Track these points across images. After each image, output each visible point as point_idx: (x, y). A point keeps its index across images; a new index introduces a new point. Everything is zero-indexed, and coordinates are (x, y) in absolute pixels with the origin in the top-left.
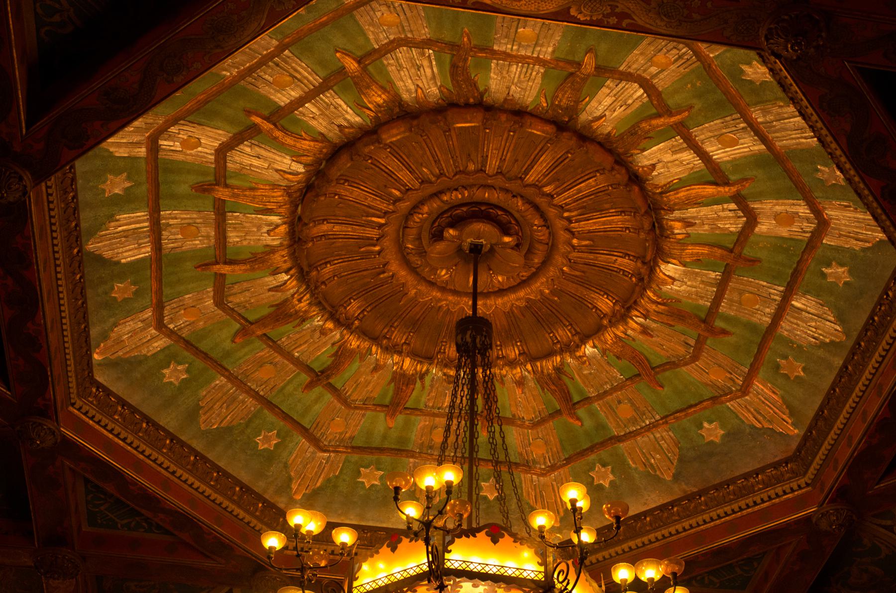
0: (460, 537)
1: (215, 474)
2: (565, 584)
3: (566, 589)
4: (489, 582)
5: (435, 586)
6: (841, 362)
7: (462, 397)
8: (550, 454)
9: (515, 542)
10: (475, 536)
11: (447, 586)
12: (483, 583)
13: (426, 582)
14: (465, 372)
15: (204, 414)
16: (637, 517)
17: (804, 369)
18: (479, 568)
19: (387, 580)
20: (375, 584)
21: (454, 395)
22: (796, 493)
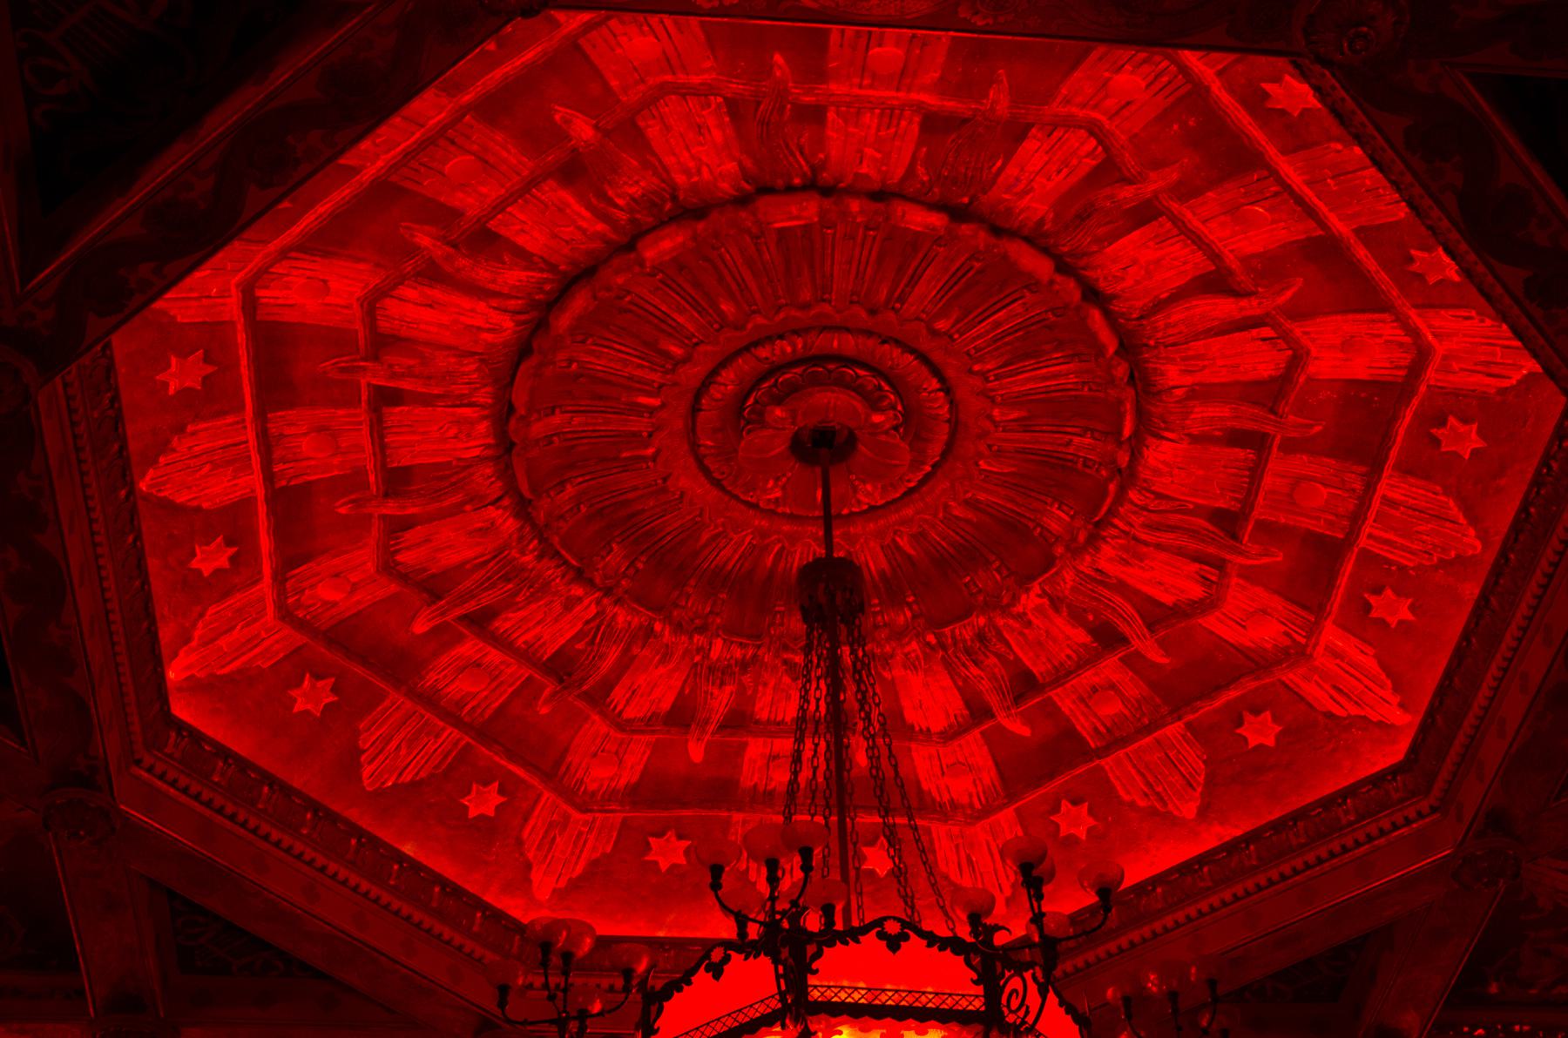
2: (1021, 1013)
3: (1023, 1022)
10: (857, 941)
11: (815, 1033)
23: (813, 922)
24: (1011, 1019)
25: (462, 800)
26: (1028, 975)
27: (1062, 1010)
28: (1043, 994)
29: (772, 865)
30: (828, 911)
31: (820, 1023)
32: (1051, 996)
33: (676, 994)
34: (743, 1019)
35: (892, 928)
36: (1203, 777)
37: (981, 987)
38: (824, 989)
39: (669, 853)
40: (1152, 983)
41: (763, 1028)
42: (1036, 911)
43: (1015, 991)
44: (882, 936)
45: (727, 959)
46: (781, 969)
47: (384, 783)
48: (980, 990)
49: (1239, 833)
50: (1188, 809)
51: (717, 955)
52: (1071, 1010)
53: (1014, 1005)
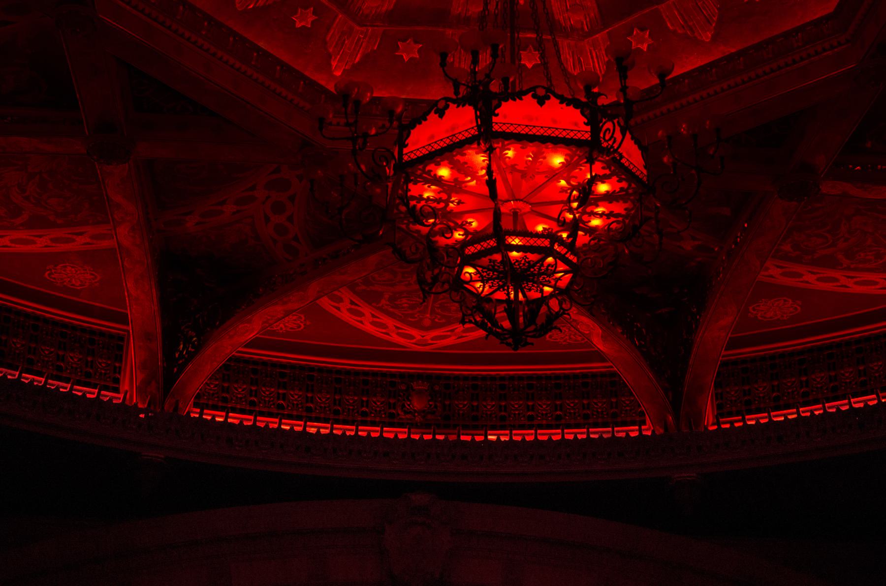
2: (610, 143)
3: (612, 147)
5: (484, 148)
8: (588, 20)
9: (561, 103)
10: (521, 99)
11: (495, 149)
12: (531, 144)
18: (527, 130)
19: (430, 147)
23: (495, 87)
24: (605, 145)
25: (292, 17)
26: (616, 121)
27: (633, 142)
28: (624, 135)
29: (475, 55)
30: (505, 81)
31: (499, 144)
32: (628, 135)
33: (417, 125)
34: (437, 147)
35: (541, 92)
36: (716, 18)
37: (589, 127)
38: (502, 125)
39: (409, 52)
40: (683, 129)
41: (467, 145)
42: (623, 84)
43: (608, 129)
44: (534, 96)
45: (447, 107)
46: (478, 113)
47: (248, 6)
48: (588, 128)
49: (733, 50)
50: (707, 36)
51: (441, 105)
52: (637, 142)
53: (607, 138)
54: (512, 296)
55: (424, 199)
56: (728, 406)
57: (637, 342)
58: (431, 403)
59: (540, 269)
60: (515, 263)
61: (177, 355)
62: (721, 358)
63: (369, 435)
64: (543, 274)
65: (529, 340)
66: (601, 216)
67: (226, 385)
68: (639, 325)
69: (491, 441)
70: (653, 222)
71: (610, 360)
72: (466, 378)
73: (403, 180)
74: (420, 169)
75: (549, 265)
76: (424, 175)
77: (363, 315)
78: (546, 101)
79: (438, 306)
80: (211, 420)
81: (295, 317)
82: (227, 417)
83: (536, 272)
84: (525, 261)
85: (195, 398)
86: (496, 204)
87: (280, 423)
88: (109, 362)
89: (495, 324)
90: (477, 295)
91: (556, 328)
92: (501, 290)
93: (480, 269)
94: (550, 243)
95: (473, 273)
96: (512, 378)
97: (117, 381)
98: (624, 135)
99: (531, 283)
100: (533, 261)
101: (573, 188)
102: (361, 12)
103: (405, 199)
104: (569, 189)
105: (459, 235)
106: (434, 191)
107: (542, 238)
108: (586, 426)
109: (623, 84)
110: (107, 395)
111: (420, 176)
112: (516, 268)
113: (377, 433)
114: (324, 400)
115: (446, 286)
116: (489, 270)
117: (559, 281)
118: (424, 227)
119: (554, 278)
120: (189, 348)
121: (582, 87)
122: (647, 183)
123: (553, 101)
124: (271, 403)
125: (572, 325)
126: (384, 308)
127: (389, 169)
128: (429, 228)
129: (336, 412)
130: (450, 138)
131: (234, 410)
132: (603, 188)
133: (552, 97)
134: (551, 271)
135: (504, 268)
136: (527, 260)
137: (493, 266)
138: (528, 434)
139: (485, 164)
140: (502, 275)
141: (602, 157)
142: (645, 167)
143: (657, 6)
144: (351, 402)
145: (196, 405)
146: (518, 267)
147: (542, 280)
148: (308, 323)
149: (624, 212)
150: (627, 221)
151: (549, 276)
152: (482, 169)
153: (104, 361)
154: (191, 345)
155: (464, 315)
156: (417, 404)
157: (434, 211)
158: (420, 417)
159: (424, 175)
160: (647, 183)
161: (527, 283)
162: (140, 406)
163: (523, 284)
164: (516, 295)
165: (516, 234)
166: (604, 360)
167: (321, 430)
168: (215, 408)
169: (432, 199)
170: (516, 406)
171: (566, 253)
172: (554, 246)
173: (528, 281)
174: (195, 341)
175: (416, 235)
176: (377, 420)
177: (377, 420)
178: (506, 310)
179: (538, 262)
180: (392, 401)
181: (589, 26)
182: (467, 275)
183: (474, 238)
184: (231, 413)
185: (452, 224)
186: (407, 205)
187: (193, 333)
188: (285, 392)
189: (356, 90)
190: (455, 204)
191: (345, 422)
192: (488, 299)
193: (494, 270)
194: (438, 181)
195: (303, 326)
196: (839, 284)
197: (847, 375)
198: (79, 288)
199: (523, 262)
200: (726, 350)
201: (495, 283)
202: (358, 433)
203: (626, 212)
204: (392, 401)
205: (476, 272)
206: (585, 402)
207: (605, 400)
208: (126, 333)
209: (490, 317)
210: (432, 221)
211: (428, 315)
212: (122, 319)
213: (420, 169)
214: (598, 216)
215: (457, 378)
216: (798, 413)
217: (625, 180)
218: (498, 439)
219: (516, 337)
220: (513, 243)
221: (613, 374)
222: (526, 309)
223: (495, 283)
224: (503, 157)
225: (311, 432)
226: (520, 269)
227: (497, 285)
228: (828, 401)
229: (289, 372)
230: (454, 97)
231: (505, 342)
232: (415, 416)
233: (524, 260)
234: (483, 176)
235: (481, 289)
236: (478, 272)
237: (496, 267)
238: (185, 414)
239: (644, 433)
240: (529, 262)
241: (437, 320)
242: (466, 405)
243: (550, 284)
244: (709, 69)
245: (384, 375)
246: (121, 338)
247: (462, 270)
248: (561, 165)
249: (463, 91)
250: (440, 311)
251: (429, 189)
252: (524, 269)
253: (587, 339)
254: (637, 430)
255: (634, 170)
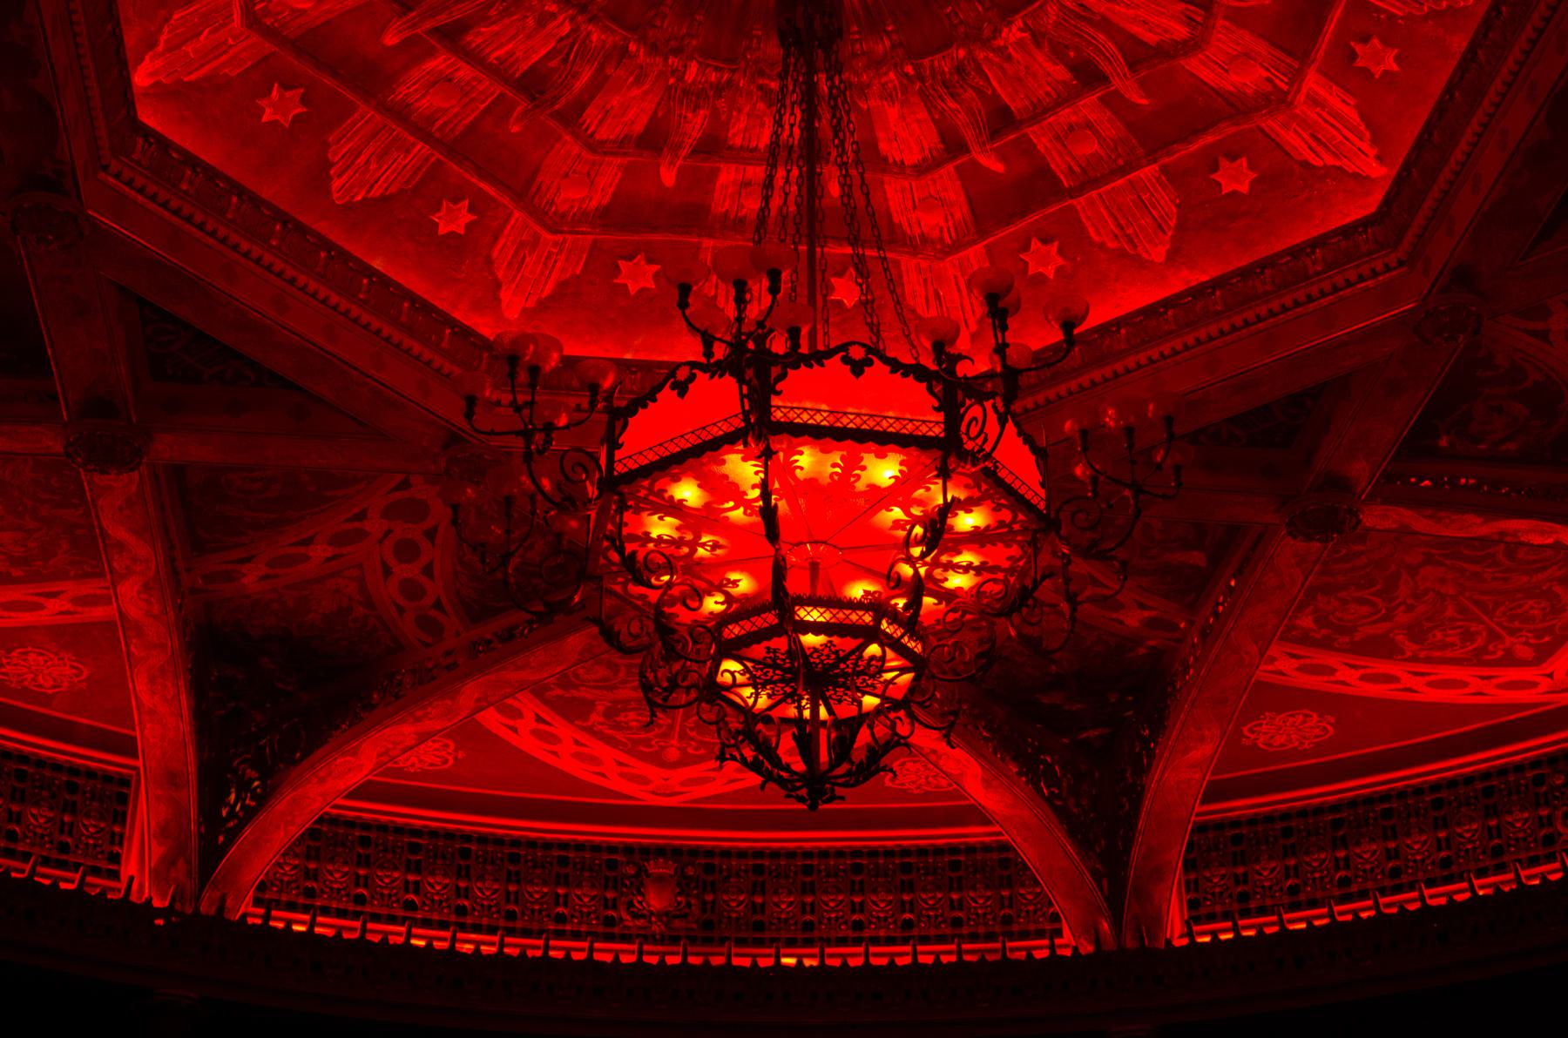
0: (796, 367)
1: (365, 281)
2: (980, 441)
3: (981, 449)
4: (849, 442)
5: (757, 452)
6: (1465, 44)
7: (792, 126)
8: (951, 223)
10: (822, 365)
11: (777, 452)
13: (741, 447)
14: (795, 81)
15: (339, 176)
16: (1105, 329)
17: (1397, 59)
20: (662, 450)
21: (779, 123)
22: (1381, 278)
23: (779, 345)
26: (988, 404)
29: (740, 287)
31: (782, 443)
35: (857, 353)
36: (1174, 221)
39: (638, 277)
40: (1110, 418)
42: (1000, 341)
44: (846, 360)
45: (692, 378)
46: (745, 390)
47: (353, 197)
48: (940, 417)
49: (1205, 278)
51: (682, 374)
54: (807, 713)
55: (652, 540)
56: (1208, 903)
57: (1045, 791)
58: (679, 899)
59: (856, 665)
60: (811, 654)
61: (224, 812)
62: (1193, 819)
63: (568, 956)
64: (862, 673)
65: (839, 791)
66: (967, 568)
67: (312, 866)
68: (1048, 759)
69: (787, 967)
70: (1061, 580)
71: (996, 821)
72: (742, 854)
73: (614, 507)
74: (644, 488)
75: (873, 657)
76: (651, 498)
77: (1298, 669)
78: (866, 369)
79: (693, 725)
80: (283, 929)
81: (437, 745)
82: (312, 924)
83: (850, 670)
84: (830, 650)
85: (257, 889)
86: (776, 550)
87: (409, 936)
88: (102, 825)
89: (776, 762)
90: (746, 711)
91: (883, 769)
92: (789, 700)
93: (749, 665)
94: (874, 619)
95: (739, 672)
96: (824, 854)
97: (115, 858)
98: (1002, 426)
99: (842, 690)
100: (844, 651)
101: (915, 521)
102: (553, 209)
103: (618, 542)
104: (907, 522)
105: (716, 603)
106: (670, 525)
107: (861, 610)
108: (956, 940)
109: (1000, 341)
110: (96, 883)
111: (645, 500)
112: (814, 663)
113: (676, 957)
114: (488, 893)
115: (693, 694)
116: (767, 666)
117: (891, 686)
118: (650, 590)
119: (882, 679)
120: (245, 799)
121: (928, 345)
122: (1045, 512)
123: (878, 369)
124: (394, 899)
125: (928, 760)
126: (595, 729)
127: (591, 483)
128: (660, 592)
129: (511, 916)
130: (698, 433)
131: (325, 911)
132: (966, 521)
133: (877, 362)
134: (880, 664)
135: (792, 663)
136: (833, 649)
137: (774, 660)
138: (853, 955)
139: (757, 479)
140: (790, 676)
141: (963, 468)
142: (1043, 485)
143: (1070, 202)
144: (537, 896)
145: (257, 902)
146: (817, 661)
147: (861, 683)
148: (461, 755)
149: (1006, 564)
150: (1012, 579)
151: (873, 677)
152: (754, 487)
153: (93, 822)
154: (249, 795)
155: (723, 746)
156: (655, 901)
157: (669, 562)
158: (659, 924)
159: (651, 498)
160: (1045, 512)
161: (834, 690)
162: (156, 904)
163: (828, 690)
164: (815, 712)
165: (815, 603)
166: (987, 822)
167: (435, 943)
168: (291, 906)
169: (666, 540)
170: (832, 904)
171: (902, 636)
172: (880, 623)
173: (836, 685)
174: (257, 787)
175: (640, 603)
176: (583, 930)
177: (584, 929)
178: (796, 738)
179: (853, 652)
180: (610, 895)
181: (953, 234)
182: (728, 677)
183: (740, 608)
184: (321, 916)
185: (699, 584)
186: (620, 550)
187: (253, 773)
188: (419, 878)
189: (532, 348)
190: (708, 548)
191: (526, 933)
192: (764, 717)
193: (775, 666)
194: (676, 508)
195: (451, 762)
196: (1399, 686)
197: (1417, 847)
198: (50, 691)
199: (826, 652)
200: (1202, 803)
201: (776, 688)
202: (548, 954)
203: (1009, 563)
204: (610, 895)
205: (742, 670)
206: (955, 896)
207: (989, 894)
208: (134, 773)
209: (767, 750)
210: (666, 578)
211: (675, 742)
212: (126, 746)
213: (644, 488)
214: (961, 571)
215: (726, 854)
216: (1331, 914)
217: (1005, 507)
218: (800, 963)
219: (816, 785)
220: (808, 618)
221: (1004, 847)
222: (833, 735)
223: (776, 688)
224: (790, 468)
225: (464, 951)
226: (820, 666)
227: (782, 692)
228: (1383, 894)
229: (426, 842)
230: (703, 360)
231: (794, 794)
232: (650, 922)
233: (827, 649)
234: (755, 500)
235: (752, 699)
236: (746, 670)
237: (779, 662)
238: (237, 918)
239: (1059, 952)
240: (836, 653)
241: (690, 750)
242: (742, 902)
243: (875, 691)
244: (1162, 310)
245: (596, 848)
246: (124, 782)
247: (719, 665)
248: (893, 480)
249: (720, 351)
250: (694, 733)
251: (662, 522)
252: (828, 664)
253: (958, 785)
254: (1046, 948)
255: (1022, 491)
